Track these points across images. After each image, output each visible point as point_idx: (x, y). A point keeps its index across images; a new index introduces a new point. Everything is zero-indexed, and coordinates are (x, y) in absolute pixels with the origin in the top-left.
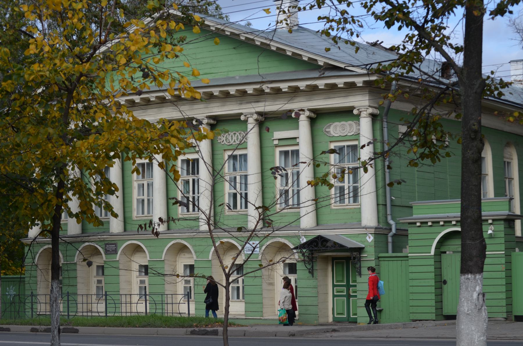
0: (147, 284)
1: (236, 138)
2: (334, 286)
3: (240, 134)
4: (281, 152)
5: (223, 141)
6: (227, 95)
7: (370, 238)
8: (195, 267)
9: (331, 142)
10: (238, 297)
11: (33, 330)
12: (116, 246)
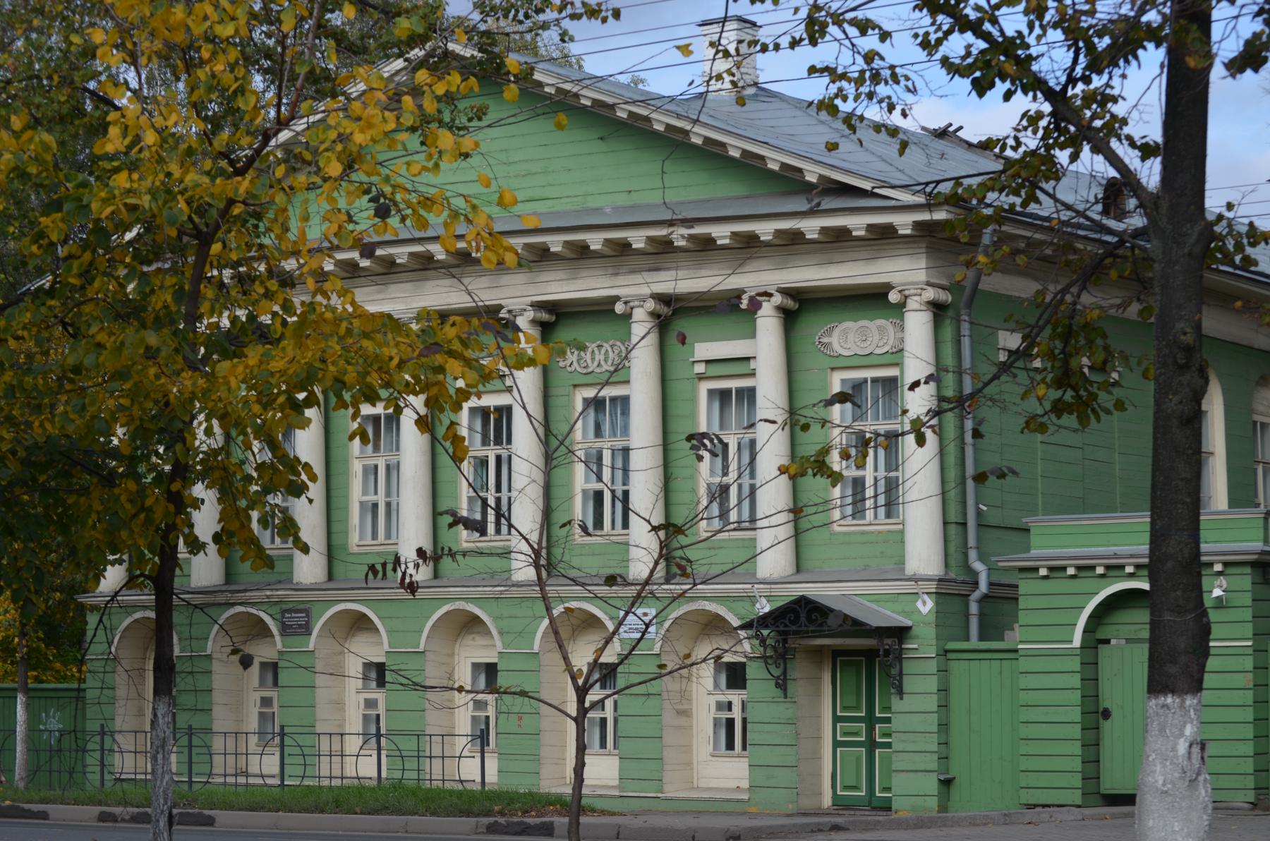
0: (381, 710)
1: (602, 358)
2: (836, 720)
3: (612, 346)
4: (711, 393)
5: (572, 363)
6: (581, 253)
7: (924, 603)
8: (499, 668)
9: (575, 386)
11: (104, 817)
12: (308, 616)
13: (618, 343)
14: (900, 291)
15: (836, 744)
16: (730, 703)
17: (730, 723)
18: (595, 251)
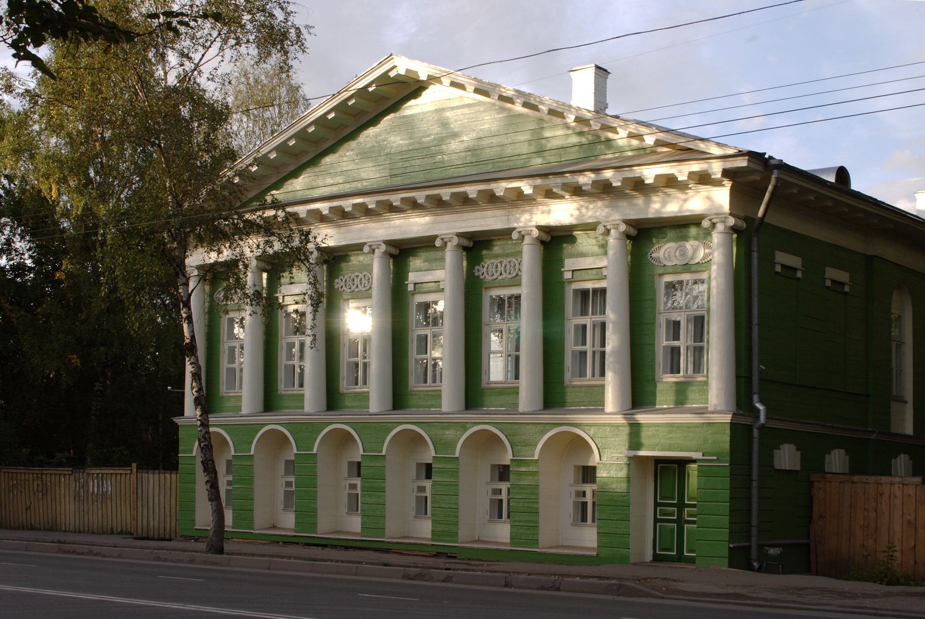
0: (428, 493)
2: (656, 505)
5: (483, 273)
8: (433, 466)
10: (500, 516)
13: (514, 260)
14: (710, 220)
15: (656, 521)
16: (584, 492)
17: (584, 505)
18: (527, 195)
